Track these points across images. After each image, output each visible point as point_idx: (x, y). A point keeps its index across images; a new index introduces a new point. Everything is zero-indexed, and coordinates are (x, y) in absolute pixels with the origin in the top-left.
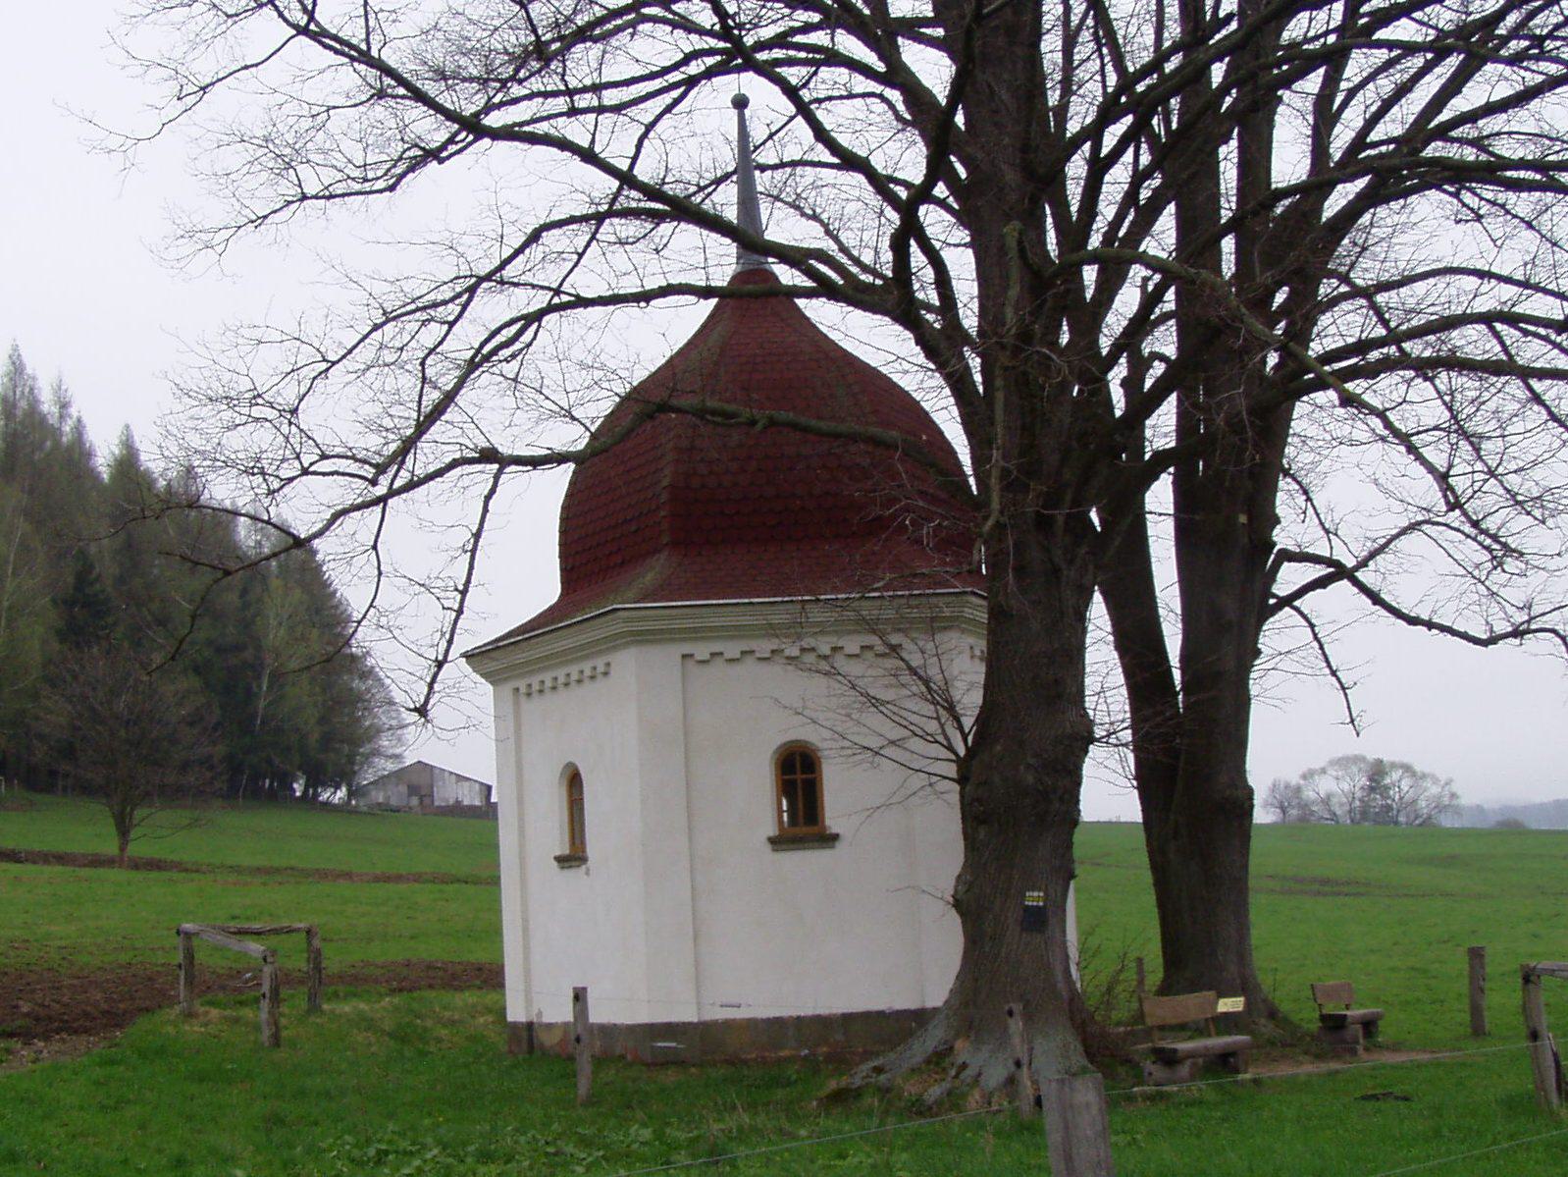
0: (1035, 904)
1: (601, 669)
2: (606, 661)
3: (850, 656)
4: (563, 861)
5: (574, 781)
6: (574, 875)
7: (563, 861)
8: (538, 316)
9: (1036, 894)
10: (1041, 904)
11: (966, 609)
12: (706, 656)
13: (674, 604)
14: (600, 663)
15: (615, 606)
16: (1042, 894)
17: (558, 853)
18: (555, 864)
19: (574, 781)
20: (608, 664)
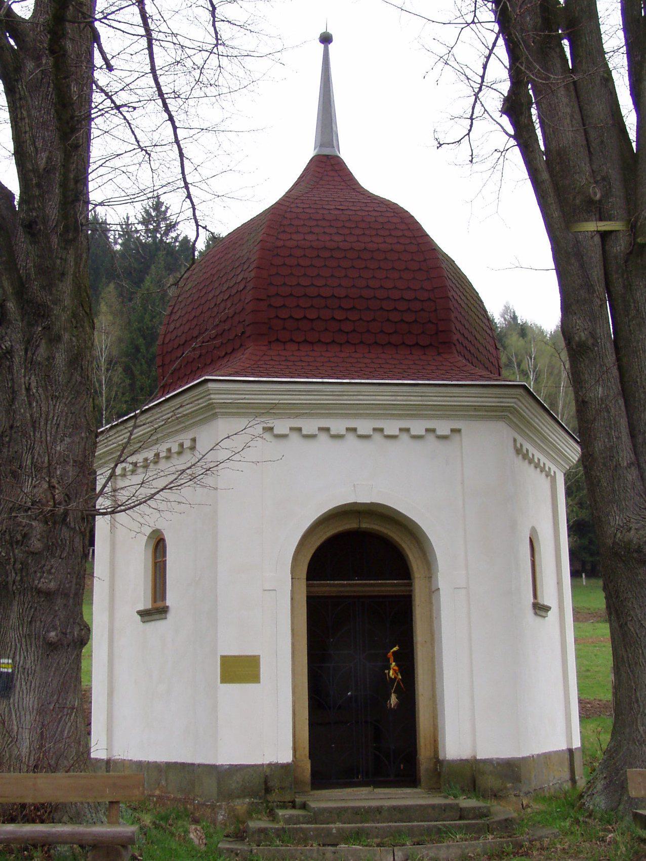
0: (6, 670)
1: (187, 444)
2: (192, 436)
3: (361, 437)
4: (146, 615)
5: (158, 545)
6: (158, 627)
7: (146, 615)
8: (223, 21)
9: (6, 661)
10: (10, 670)
11: (212, 396)
12: (447, 432)
13: (344, 381)
14: (185, 438)
15: (207, 377)
16: (10, 661)
17: (141, 607)
18: (139, 617)
19: (158, 545)
20: (194, 440)
